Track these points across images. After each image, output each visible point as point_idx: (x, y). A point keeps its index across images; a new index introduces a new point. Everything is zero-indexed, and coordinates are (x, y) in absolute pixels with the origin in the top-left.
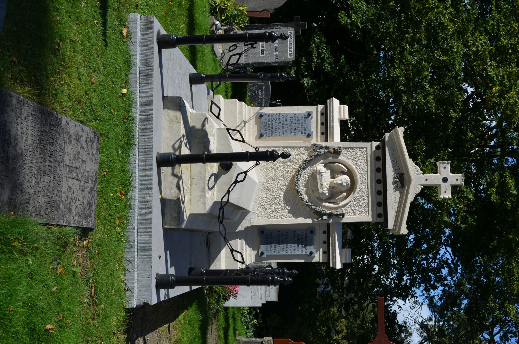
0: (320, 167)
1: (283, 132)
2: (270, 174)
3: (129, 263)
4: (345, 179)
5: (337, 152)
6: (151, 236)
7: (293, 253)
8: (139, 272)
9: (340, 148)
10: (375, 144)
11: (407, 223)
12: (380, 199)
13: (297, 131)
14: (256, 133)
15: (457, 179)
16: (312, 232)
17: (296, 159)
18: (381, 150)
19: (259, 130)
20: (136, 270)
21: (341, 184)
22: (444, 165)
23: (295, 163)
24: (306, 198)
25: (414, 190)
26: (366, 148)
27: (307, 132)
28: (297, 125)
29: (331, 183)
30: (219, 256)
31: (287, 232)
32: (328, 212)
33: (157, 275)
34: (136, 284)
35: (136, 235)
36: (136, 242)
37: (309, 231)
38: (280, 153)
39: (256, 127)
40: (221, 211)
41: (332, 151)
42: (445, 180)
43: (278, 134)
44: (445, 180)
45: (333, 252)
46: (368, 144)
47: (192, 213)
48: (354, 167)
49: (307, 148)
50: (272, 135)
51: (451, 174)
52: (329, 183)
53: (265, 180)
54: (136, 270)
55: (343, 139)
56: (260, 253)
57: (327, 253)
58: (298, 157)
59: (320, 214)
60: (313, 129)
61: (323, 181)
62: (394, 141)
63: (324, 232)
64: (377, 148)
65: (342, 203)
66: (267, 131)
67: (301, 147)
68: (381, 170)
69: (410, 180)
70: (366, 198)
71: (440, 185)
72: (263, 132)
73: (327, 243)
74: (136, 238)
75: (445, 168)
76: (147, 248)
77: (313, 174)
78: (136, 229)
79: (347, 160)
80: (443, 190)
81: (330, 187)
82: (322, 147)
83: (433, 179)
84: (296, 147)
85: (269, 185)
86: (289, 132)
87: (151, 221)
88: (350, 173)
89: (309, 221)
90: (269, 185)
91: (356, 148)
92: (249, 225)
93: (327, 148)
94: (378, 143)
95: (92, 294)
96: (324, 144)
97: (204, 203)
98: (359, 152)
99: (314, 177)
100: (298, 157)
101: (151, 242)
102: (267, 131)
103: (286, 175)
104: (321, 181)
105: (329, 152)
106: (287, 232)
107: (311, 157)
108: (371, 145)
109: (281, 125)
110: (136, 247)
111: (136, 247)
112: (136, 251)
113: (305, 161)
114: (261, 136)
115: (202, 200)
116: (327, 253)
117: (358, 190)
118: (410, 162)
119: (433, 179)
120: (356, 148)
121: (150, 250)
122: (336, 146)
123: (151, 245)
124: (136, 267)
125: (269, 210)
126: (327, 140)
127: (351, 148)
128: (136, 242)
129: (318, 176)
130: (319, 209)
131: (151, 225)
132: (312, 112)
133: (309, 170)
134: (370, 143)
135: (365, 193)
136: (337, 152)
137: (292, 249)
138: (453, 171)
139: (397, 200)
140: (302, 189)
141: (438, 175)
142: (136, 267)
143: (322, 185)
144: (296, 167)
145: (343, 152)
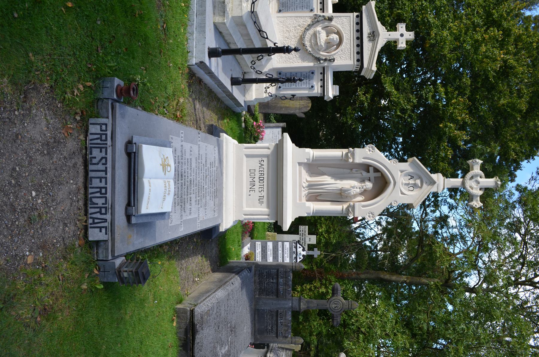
0: (319, 28)
1: (294, 8)
2: (285, 35)
3: (190, 35)
4: (335, 37)
5: (330, 19)
6: (205, 18)
7: (300, 87)
8: (197, 42)
9: (332, 16)
10: (356, 14)
11: (377, 63)
12: (358, 27)
13: (303, 8)
14: (277, 9)
15: (410, 36)
16: (313, 73)
17: (303, 24)
18: (359, 18)
19: (279, 7)
20: (195, 39)
21: (333, 39)
22: (401, 26)
23: (303, 27)
24: (310, 49)
25: (381, 43)
26: (350, 17)
27: (311, 8)
28: (304, 4)
29: (326, 40)
30: (251, 88)
31: (296, 73)
32: (324, 58)
33: (209, 48)
34: (195, 49)
35: (195, 17)
36: (195, 22)
37: (311, 72)
38: (293, 47)
39: (277, 4)
40: (253, 5)
41: (327, 18)
42: (402, 35)
43: (291, 10)
44: (402, 35)
45: (327, 85)
46: (351, 14)
47: (233, 15)
48: (341, 29)
49: (310, 17)
50: (287, 11)
51: (406, 32)
52: (325, 40)
53: (282, 39)
54: (195, 39)
55: (334, 12)
56: (278, 87)
57: (323, 87)
58: (305, 23)
59: (318, 59)
60: (315, 6)
61: (321, 39)
62: (369, 11)
63: (321, 73)
64: (357, 16)
65: (333, 53)
66: (284, 8)
67: (307, 17)
68: (360, 31)
69: (379, 35)
70: (350, 49)
71: (398, 39)
72: (281, 9)
73: (323, 80)
74: (195, 20)
75: (402, 27)
76: (203, 25)
77: (314, 33)
78: (195, 13)
79: (336, 25)
80: (400, 42)
81: (325, 43)
82: (320, 16)
83: (394, 35)
84: (303, 17)
85: (285, 42)
86: (298, 8)
87: (205, 8)
88: (338, 33)
89: (311, 64)
90: (285, 42)
91: (343, 17)
92: (271, 68)
93: (323, 16)
94: (357, 14)
95: (164, 27)
96: (322, 14)
97: (241, 9)
98: (345, 20)
99: (315, 35)
100: (305, 23)
101: (205, 21)
102: (284, 8)
103: (296, 35)
104: (319, 38)
105: (325, 19)
106: (296, 73)
107: (313, 22)
108: (353, 15)
109: (293, 4)
110: (195, 25)
111: (195, 25)
112: (195, 28)
113: (309, 25)
114: (280, 11)
115: (240, 7)
116: (323, 87)
117: (344, 44)
118: (379, 24)
119: (394, 35)
120: (343, 17)
121: (205, 27)
122: (330, 15)
123: (205, 24)
124: (195, 38)
125: (285, 58)
126: (323, 12)
127: (340, 17)
128: (195, 22)
129: (317, 35)
130: (318, 56)
131: (205, 11)
132: (314, 12)
133: (311, 32)
134: (352, 13)
135: (348, 46)
136: (330, 19)
137: (300, 85)
138: (408, 29)
139: (370, 49)
140: (307, 44)
141: (398, 32)
142: (195, 38)
143: (320, 40)
144: (303, 29)
145: (334, 19)
